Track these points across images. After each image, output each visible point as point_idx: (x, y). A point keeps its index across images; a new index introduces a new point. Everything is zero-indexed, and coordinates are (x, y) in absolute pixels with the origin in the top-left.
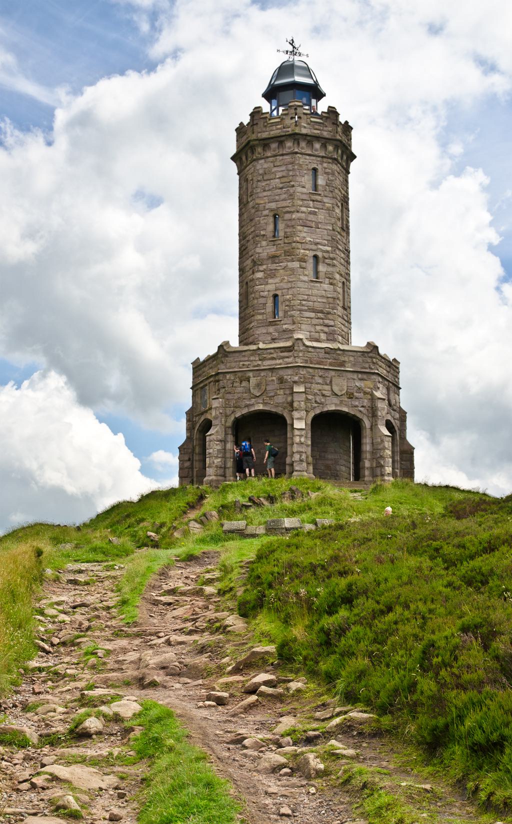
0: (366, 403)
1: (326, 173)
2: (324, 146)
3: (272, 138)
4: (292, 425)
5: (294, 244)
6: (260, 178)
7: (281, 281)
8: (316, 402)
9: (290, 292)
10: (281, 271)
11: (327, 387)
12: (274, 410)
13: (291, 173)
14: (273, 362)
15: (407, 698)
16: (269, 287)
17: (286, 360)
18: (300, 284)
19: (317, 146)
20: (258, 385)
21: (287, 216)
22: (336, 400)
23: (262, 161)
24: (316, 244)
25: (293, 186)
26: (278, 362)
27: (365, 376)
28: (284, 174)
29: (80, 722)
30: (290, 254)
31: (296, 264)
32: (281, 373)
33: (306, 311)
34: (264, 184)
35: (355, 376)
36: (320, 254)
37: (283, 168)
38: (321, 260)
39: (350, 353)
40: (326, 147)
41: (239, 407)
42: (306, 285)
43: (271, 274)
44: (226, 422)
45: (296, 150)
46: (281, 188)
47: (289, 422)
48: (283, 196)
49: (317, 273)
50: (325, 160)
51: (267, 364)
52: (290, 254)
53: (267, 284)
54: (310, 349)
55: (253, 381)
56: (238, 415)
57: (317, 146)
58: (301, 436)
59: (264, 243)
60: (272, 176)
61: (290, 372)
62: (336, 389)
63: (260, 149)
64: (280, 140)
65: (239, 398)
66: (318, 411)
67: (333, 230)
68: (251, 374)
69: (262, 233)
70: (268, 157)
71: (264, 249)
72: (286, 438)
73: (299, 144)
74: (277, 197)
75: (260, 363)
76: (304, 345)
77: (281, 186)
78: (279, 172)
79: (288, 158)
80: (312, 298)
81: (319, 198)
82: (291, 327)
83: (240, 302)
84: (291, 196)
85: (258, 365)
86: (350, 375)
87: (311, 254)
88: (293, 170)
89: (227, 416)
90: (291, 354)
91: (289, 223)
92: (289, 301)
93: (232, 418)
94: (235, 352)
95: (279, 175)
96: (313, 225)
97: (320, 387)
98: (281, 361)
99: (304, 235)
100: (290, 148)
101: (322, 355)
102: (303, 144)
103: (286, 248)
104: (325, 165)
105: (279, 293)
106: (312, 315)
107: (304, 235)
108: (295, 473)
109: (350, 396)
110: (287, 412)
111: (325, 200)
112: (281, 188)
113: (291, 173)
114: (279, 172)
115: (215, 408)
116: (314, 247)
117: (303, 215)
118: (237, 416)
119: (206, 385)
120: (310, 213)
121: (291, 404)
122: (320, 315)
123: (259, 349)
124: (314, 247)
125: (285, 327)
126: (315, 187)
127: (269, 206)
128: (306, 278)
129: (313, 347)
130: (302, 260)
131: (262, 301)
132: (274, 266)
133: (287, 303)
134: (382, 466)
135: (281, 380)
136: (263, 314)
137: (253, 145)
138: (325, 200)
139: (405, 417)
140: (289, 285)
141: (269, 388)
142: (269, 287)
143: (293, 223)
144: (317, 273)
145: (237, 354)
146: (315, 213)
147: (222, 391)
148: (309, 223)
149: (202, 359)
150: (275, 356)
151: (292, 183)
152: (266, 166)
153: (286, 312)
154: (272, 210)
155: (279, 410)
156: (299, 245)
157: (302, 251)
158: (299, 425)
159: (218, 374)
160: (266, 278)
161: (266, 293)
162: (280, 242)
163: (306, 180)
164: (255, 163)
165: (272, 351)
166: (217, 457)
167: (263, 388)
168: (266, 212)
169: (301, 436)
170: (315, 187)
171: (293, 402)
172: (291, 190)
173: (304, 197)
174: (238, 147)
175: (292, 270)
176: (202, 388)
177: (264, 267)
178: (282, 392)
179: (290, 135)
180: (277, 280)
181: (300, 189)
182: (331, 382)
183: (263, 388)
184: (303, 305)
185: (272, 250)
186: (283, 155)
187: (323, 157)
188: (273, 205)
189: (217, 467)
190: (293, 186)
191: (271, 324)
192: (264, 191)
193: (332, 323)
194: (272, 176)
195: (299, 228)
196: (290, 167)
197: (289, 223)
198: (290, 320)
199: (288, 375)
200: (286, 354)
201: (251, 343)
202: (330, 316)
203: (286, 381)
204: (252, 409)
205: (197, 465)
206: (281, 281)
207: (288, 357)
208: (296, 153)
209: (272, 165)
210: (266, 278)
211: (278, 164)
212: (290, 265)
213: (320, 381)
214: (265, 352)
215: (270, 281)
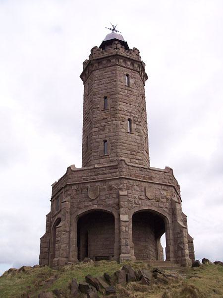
0: (168, 205)
2: (132, 64)
3: (103, 58)
4: (119, 218)
8: (135, 203)
9: (115, 137)
14: (105, 176)
16: (101, 136)
19: (129, 63)
21: (112, 97)
23: (98, 71)
24: (130, 112)
25: (116, 81)
26: (108, 175)
27: (166, 188)
29: (101, 278)
32: (110, 183)
35: (160, 187)
36: (132, 118)
38: (133, 122)
39: (157, 172)
40: (133, 65)
41: (80, 208)
42: (124, 135)
51: (100, 177)
54: (130, 167)
57: (129, 63)
58: (126, 226)
61: (117, 181)
62: (149, 195)
63: (96, 65)
65: (80, 201)
66: (137, 210)
67: (139, 107)
68: (88, 185)
71: (98, 115)
72: (114, 229)
76: (126, 164)
80: (127, 142)
81: (130, 89)
83: (83, 149)
86: (157, 186)
87: (127, 118)
94: (78, 171)
95: (107, 76)
96: (128, 102)
97: (138, 193)
98: (110, 175)
99: (123, 107)
101: (138, 172)
108: (122, 255)
111: (134, 91)
116: (129, 114)
118: (78, 214)
119: (59, 196)
120: (126, 96)
121: (118, 204)
123: (95, 168)
128: (124, 131)
129: (132, 166)
133: (113, 145)
134: (183, 250)
135: (111, 188)
138: (134, 91)
139: (186, 219)
145: (79, 172)
150: (105, 172)
152: (99, 73)
158: (124, 218)
159: (66, 186)
165: (104, 169)
169: (126, 226)
171: (119, 202)
179: (114, 56)
182: (145, 189)
185: (104, 115)
187: (132, 69)
190: (116, 81)
191: (102, 157)
192: (98, 85)
193: (140, 158)
201: (90, 166)
202: (139, 154)
205: (51, 249)
208: (117, 65)
215: (102, 132)
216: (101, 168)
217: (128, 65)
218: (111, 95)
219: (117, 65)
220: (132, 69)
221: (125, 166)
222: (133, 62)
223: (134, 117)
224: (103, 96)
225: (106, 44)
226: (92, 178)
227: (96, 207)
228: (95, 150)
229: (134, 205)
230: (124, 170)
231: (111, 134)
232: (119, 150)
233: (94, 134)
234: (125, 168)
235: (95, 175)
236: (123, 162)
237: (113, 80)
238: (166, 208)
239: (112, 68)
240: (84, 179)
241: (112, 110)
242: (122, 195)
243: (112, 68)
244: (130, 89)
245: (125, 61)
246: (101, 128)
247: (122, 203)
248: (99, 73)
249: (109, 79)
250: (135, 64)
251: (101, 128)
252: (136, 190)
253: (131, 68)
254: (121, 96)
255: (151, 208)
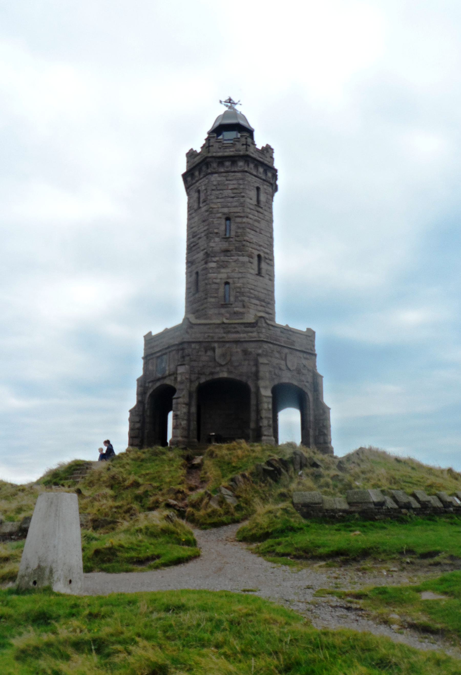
1: (266, 193)
5: (244, 243)
6: (214, 188)
7: (233, 271)
9: (241, 281)
10: (233, 264)
11: (283, 362)
12: (238, 378)
13: (242, 187)
15: (324, 655)
16: (220, 276)
17: (250, 334)
18: (249, 276)
20: (224, 355)
21: (239, 220)
22: (289, 374)
24: (260, 246)
25: (243, 197)
26: (242, 335)
28: (236, 186)
30: (241, 249)
31: (246, 259)
32: (246, 345)
33: (253, 298)
34: (218, 192)
36: (262, 255)
37: (234, 182)
38: (263, 259)
39: (233, 326)
41: (204, 374)
43: (222, 265)
44: (190, 387)
45: (246, 169)
46: (233, 197)
47: (253, 389)
48: (235, 204)
49: (260, 269)
50: (266, 183)
52: (241, 249)
53: (219, 273)
55: (218, 351)
56: (203, 380)
57: (261, 170)
59: (217, 239)
60: (226, 187)
61: (253, 345)
62: (289, 365)
63: (215, 165)
64: (233, 159)
68: (216, 345)
69: (216, 231)
70: (222, 172)
73: (248, 165)
74: (229, 204)
75: (225, 335)
77: (233, 195)
78: (232, 184)
79: (239, 175)
82: (241, 310)
84: (242, 205)
85: (223, 337)
87: (256, 253)
88: (244, 184)
89: (191, 381)
90: (254, 329)
91: (240, 225)
92: (240, 288)
93: (196, 384)
95: (230, 187)
96: (258, 230)
98: (245, 335)
99: (252, 236)
100: (241, 167)
102: (252, 166)
103: (237, 245)
104: (265, 187)
105: (230, 281)
106: (257, 302)
107: (252, 236)
109: (299, 371)
110: (219, 389)
112: (233, 197)
113: (242, 187)
114: (232, 184)
115: (181, 374)
117: (251, 220)
120: (256, 220)
122: (263, 304)
123: (223, 323)
124: (259, 248)
125: (236, 309)
126: (258, 201)
127: (221, 210)
128: (252, 271)
130: (250, 256)
131: (214, 286)
132: (226, 259)
133: (238, 290)
135: (245, 352)
136: (215, 297)
137: (200, 169)
140: (240, 275)
141: (234, 358)
142: (220, 276)
143: (243, 225)
144: (260, 269)
146: (259, 222)
147: (187, 358)
148: (255, 228)
149: (154, 333)
151: (243, 194)
152: (219, 179)
153: (236, 297)
154: (224, 214)
155: (244, 379)
156: (248, 244)
157: (250, 249)
160: (218, 268)
161: (218, 281)
162: (231, 239)
163: (253, 194)
164: (210, 176)
165: (236, 326)
166: (183, 419)
167: (228, 358)
168: (220, 215)
170: (258, 201)
172: (242, 200)
173: (252, 207)
174: (188, 166)
175: (243, 263)
176: (158, 357)
177: (217, 259)
178: (246, 363)
180: (229, 270)
181: (248, 200)
182: (286, 357)
183: (228, 358)
184: (251, 293)
186: (234, 172)
187: (264, 180)
188: (226, 210)
189: (183, 428)
190: (243, 197)
192: (218, 198)
194: (226, 187)
195: (248, 230)
196: (241, 182)
197: (240, 225)
198: (240, 304)
199: (251, 347)
200: (249, 329)
203: (250, 353)
204: (216, 377)
206: (233, 271)
207: (251, 332)
208: (246, 172)
209: (224, 179)
210: (218, 268)
211: (231, 178)
212: (241, 259)
213: (277, 355)
214: (230, 326)
215: (223, 270)
216: (232, 324)
217: (260, 173)
218: (236, 217)
219: (246, 172)
220: (264, 180)
221: (264, 325)
222: (258, 163)
223: (265, 253)
224: (224, 217)
225: (219, 130)
226: (220, 335)
227: (225, 375)
228: (213, 295)
229: (274, 377)
230: (264, 330)
231: (236, 275)
232: (246, 299)
233: (211, 271)
234: (264, 327)
235: (224, 333)
236: (263, 320)
237: (238, 194)
238: (307, 382)
239: (229, 171)
240: (209, 336)
241: (237, 239)
242: (262, 364)
243: (229, 171)
244: (260, 210)
245: (256, 167)
246: (221, 263)
247: (261, 374)
248: (219, 179)
249: (235, 191)
250: (262, 166)
251: (221, 263)
252: (276, 358)
253: (264, 177)
254: (250, 221)
255: (291, 381)
